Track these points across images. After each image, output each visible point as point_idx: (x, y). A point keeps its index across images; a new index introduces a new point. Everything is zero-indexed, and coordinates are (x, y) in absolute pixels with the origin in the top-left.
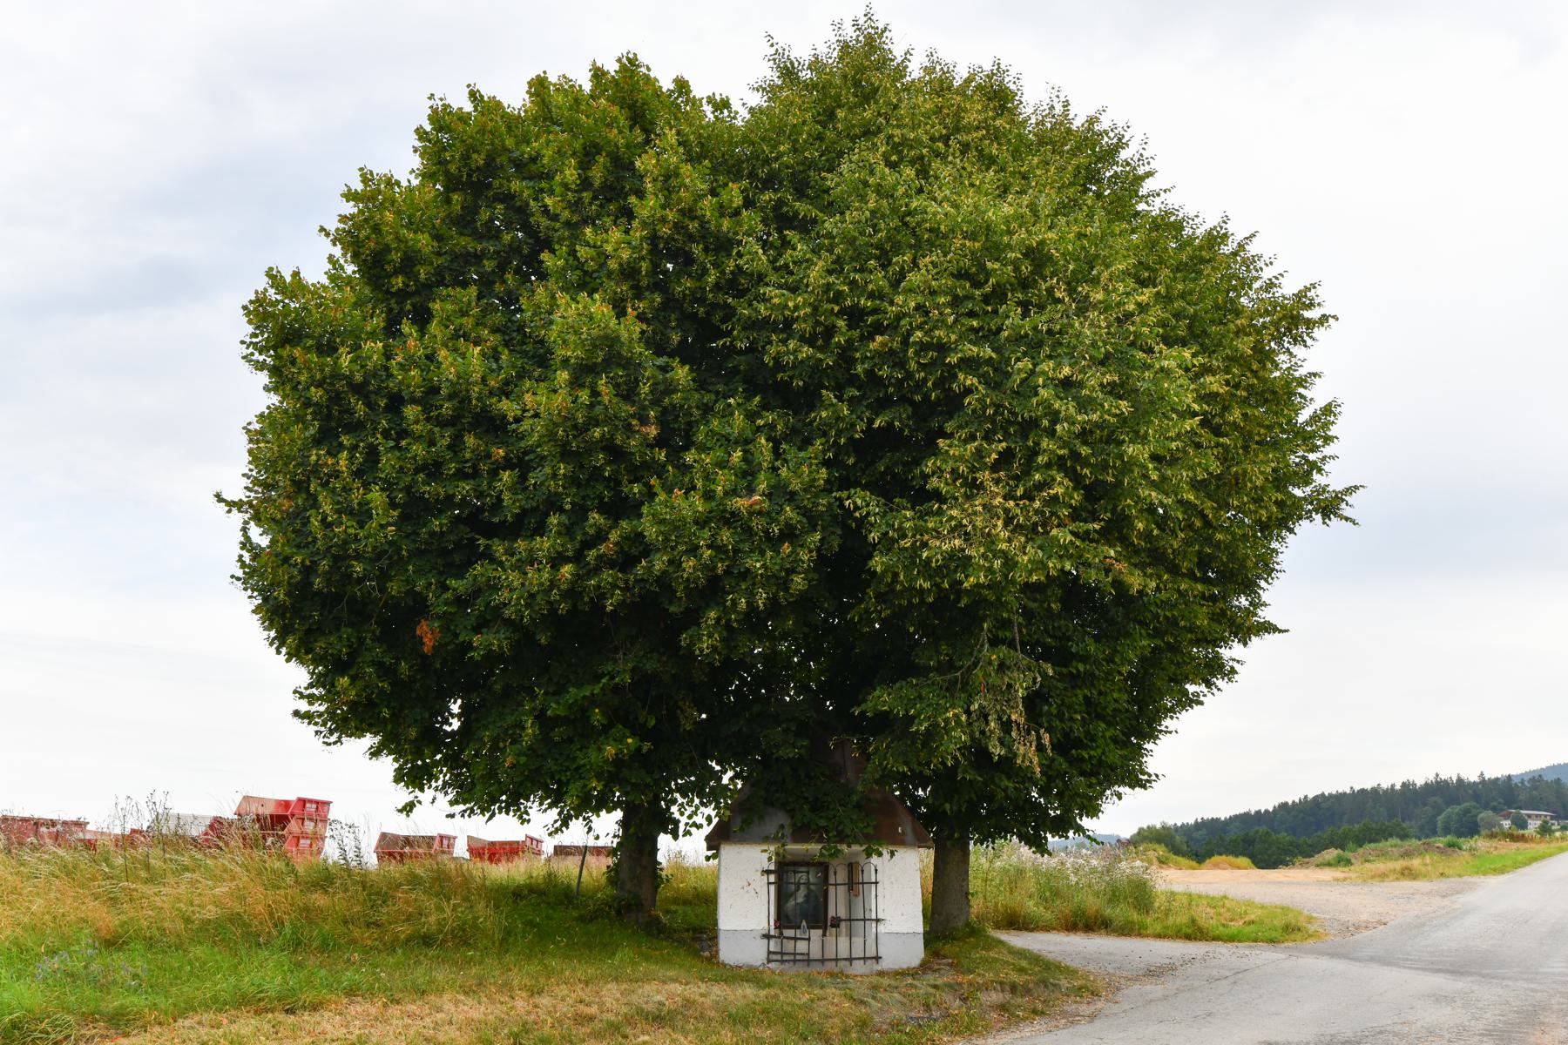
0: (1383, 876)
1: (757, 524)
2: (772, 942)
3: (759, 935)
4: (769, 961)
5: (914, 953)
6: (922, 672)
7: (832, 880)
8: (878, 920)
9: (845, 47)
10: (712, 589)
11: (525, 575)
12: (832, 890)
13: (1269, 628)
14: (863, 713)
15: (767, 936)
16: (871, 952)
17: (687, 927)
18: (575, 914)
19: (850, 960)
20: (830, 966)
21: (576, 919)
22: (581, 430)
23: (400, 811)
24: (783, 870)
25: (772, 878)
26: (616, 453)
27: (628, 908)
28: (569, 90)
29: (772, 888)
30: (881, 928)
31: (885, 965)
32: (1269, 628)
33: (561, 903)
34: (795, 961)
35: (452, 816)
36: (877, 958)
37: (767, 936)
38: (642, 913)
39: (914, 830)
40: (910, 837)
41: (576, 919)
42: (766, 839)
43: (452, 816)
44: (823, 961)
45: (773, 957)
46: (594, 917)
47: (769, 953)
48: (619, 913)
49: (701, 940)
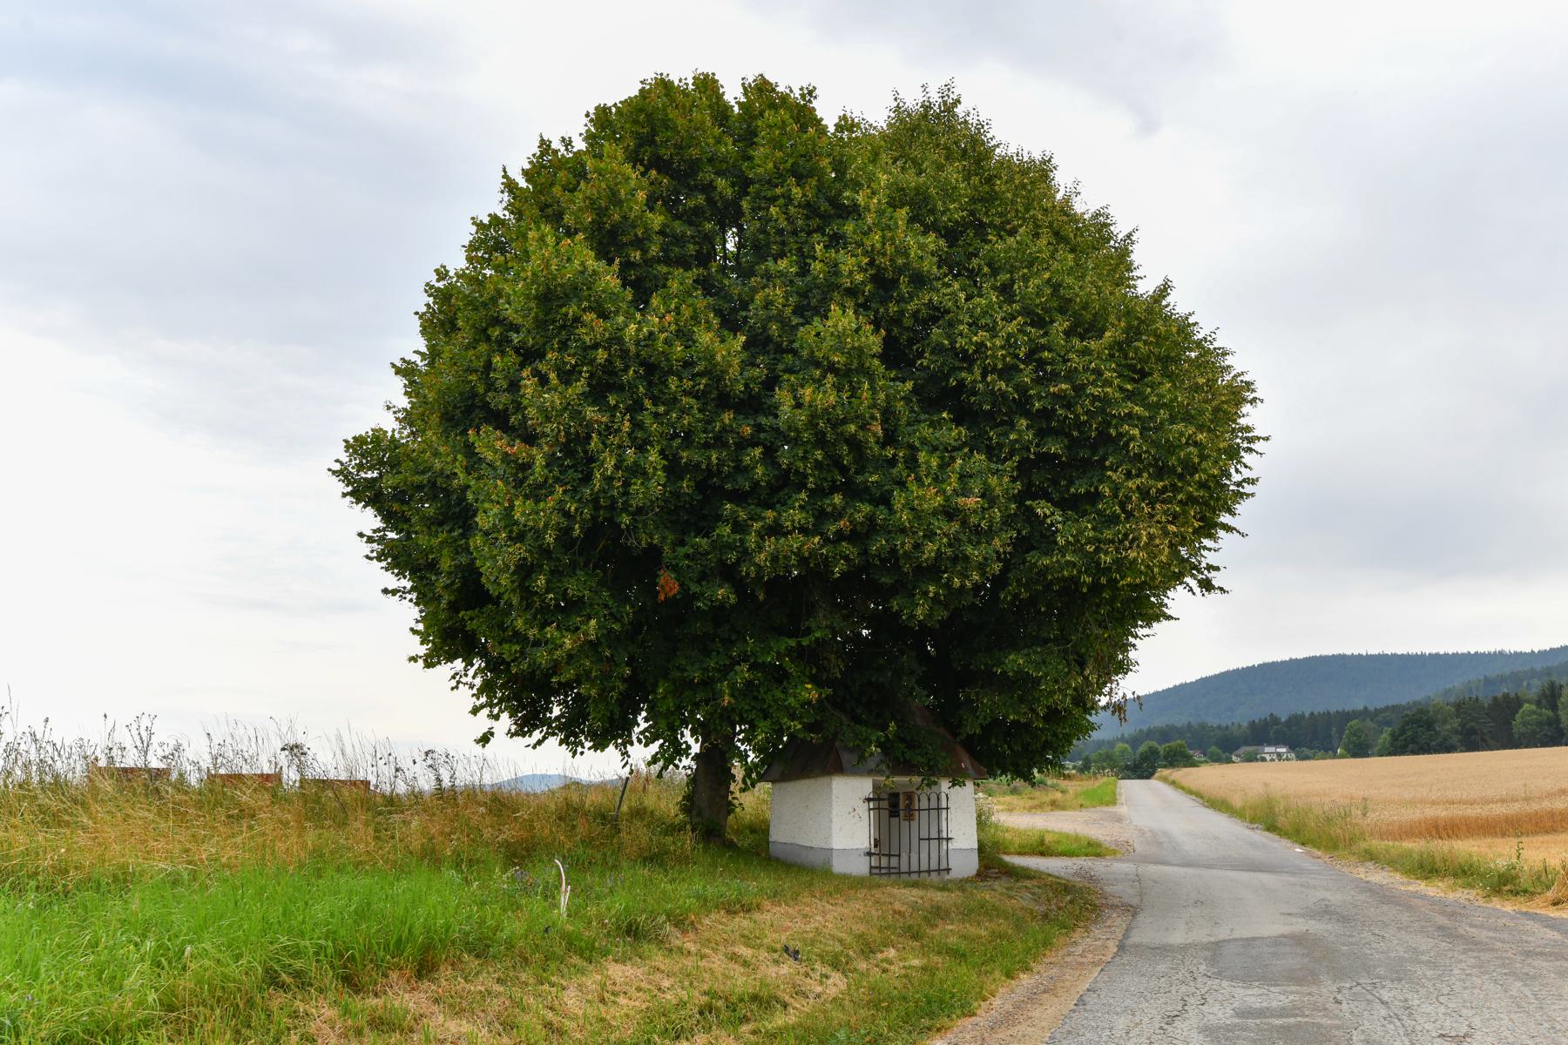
0: (1040, 807)
1: (973, 520)
5: (861, 867)
6: (1046, 641)
8: (948, 839)
9: (927, 107)
10: (932, 571)
11: (781, 540)
13: (1169, 618)
14: (1004, 673)
15: (869, 854)
16: (943, 866)
17: (755, 850)
19: (929, 871)
20: (914, 877)
22: (836, 424)
23: (478, 742)
24: (876, 798)
26: (855, 445)
28: (1050, 190)
31: (954, 874)
32: (1169, 618)
34: (889, 874)
36: (948, 870)
37: (869, 854)
40: (971, 772)
42: (870, 772)
44: (909, 873)
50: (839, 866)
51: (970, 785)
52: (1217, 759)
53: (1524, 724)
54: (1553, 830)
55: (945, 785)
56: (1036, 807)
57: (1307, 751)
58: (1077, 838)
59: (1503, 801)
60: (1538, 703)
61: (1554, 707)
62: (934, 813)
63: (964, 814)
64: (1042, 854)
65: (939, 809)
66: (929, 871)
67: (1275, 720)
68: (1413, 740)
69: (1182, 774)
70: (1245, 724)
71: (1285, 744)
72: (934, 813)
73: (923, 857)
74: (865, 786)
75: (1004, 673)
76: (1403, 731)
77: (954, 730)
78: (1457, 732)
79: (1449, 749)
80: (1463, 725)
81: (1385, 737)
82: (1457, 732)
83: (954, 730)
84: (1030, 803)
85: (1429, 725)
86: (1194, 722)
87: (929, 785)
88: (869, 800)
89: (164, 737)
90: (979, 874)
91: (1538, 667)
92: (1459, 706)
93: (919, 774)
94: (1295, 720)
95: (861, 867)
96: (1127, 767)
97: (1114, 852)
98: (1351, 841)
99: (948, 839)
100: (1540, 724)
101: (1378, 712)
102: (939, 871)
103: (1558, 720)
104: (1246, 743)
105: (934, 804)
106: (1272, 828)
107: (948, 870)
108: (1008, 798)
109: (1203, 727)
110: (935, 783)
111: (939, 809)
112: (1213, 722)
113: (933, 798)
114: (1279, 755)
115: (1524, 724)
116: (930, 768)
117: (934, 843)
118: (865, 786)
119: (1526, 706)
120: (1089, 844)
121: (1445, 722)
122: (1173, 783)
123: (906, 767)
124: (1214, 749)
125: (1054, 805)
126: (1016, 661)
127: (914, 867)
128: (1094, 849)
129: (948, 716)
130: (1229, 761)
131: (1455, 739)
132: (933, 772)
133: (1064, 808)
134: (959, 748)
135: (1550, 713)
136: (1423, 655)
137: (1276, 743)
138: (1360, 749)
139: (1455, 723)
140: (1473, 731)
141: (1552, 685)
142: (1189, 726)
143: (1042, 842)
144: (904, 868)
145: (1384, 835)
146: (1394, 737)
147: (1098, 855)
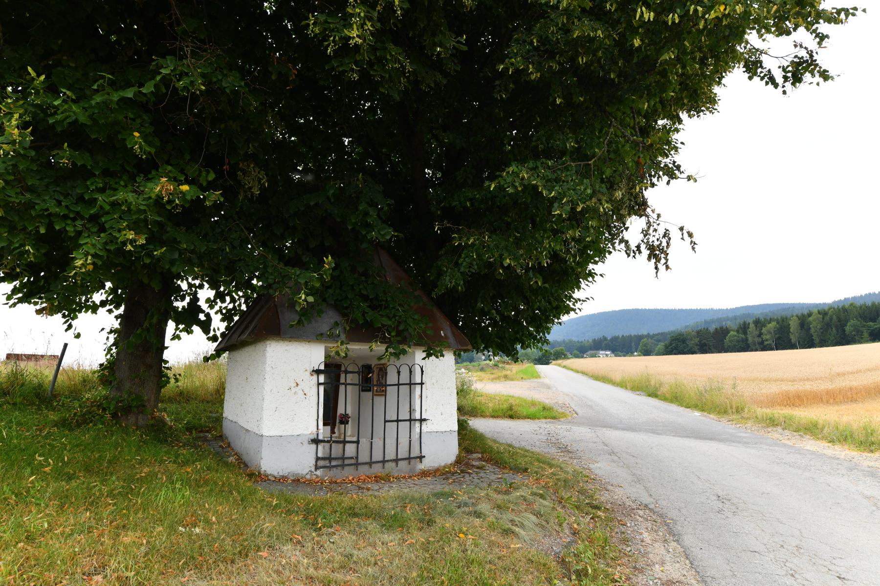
0: (498, 378)
2: (320, 447)
3: (306, 440)
4: (317, 468)
7: (342, 380)
8: (422, 420)
12: (342, 388)
15: (316, 441)
16: (415, 453)
17: (201, 432)
18: (53, 416)
21: (56, 424)
24: (332, 373)
25: (322, 379)
27: (127, 410)
29: (322, 388)
30: (424, 424)
31: (428, 463)
33: (32, 404)
35: (682, 143)
37: (316, 441)
38: (137, 417)
39: (453, 333)
40: (452, 340)
41: (56, 424)
42: (319, 337)
43: (682, 143)
44: (370, 464)
45: (321, 463)
46: (84, 420)
47: (318, 459)
48: (114, 416)
49: (205, 440)
50: (271, 463)
51: (449, 358)
52: (577, 357)
53: (730, 341)
54: (854, 400)
55: (419, 355)
56: (496, 379)
57: (620, 353)
58: (533, 404)
59: (793, 381)
60: (738, 331)
61: (745, 333)
62: (404, 389)
63: (439, 388)
64: (511, 417)
65: (411, 384)
66: (396, 461)
67: (605, 339)
68: (676, 349)
69: (559, 362)
70: (590, 341)
71: (609, 350)
72: (404, 389)
73: (390, 442)
74: (314, 355)
75: (500, 188)
76: (671, 344)
77: (428, 287)
78: (697, 345)
79: (693, 353)
80: (700, 342)
81: (661, 346)
82: (697, 345)
83: (428, 287)
84: (493, 376)
85: (684, 341)
86: (566, 339)
87: (397, 355)
88: (318, 372)
89: (207, 352)
90: (458, 461)
91: (730, 315)
92: (698, 332)
93: (383, 341)
94: (615, 339)
95: (301, 461)
96: (535, 360)
97: (564, 415)
98: (739, 410)
99: (422, 420)
100: (738, 341)
101: (654, 335)
102: (409, 459)
103: (747, 340)
104: (591, 349)
105: (404, 379)
106: (653, 394)
107: (421, 458)
108: (479, 373)
109: (571, 341)
110: (404, 352)
111: (411, 384)
112: (575, 339)
113: (405, 371)
114: (607, 355)
115: (730, 341)
116: (399, 333)
117: (404, 426)
118: (314, 355)
119: (732, 333)
120: (544, 408)
121: (691, 339)
122: (564, 367)
123: (363, 331)
124: (576, 352)
125: (506, 377)
126: (518, 175)
127: (377, 456)
128: (547, 413)
129: (420, 248)
130: (582, 357)
131: (696, 348)
132: (401, 339)
133: (512, 380)
134: (438, 314)
135: (743, 336)
136: (675, 310)
137: (606, 350)
138: (647, 353)
139: (697, 340)
140: (705, 345)
141: (745, 323)
142: (564, 341)
143: (511, 408)
144: (364, 457)
145: (761, 403)
146: (666, 347)
147: (554, 418)
